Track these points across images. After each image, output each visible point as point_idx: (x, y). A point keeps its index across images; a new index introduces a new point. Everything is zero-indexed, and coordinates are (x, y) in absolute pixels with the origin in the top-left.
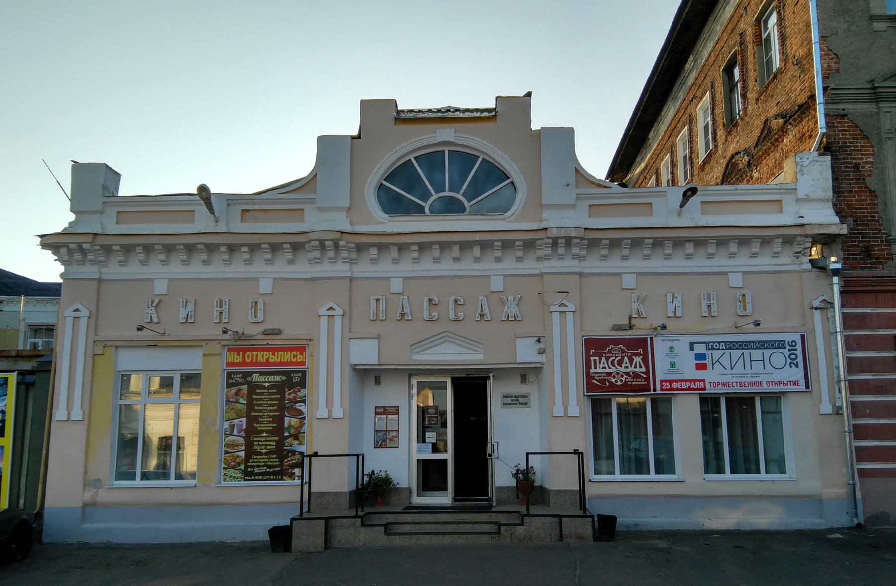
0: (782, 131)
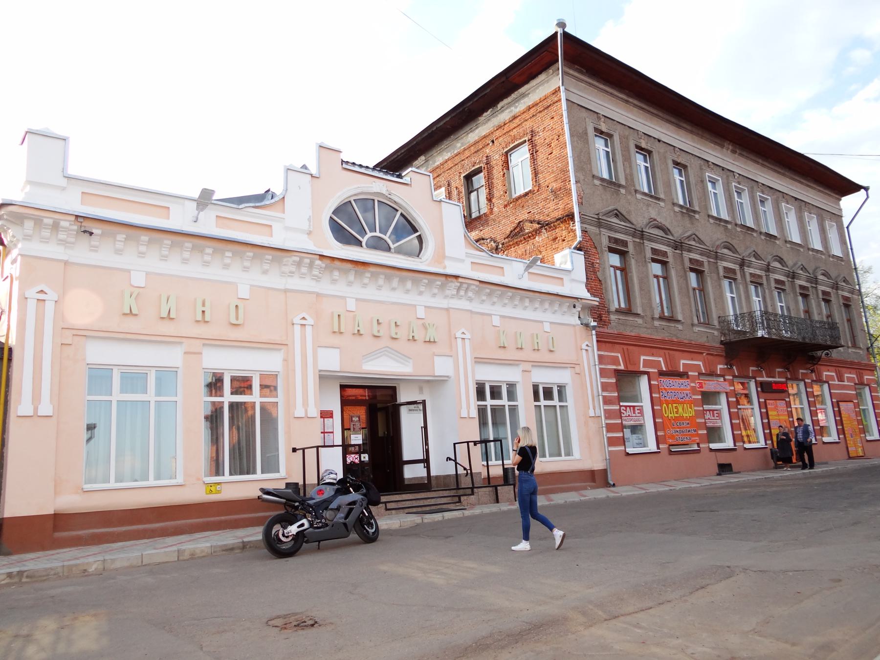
0: (536, 233)
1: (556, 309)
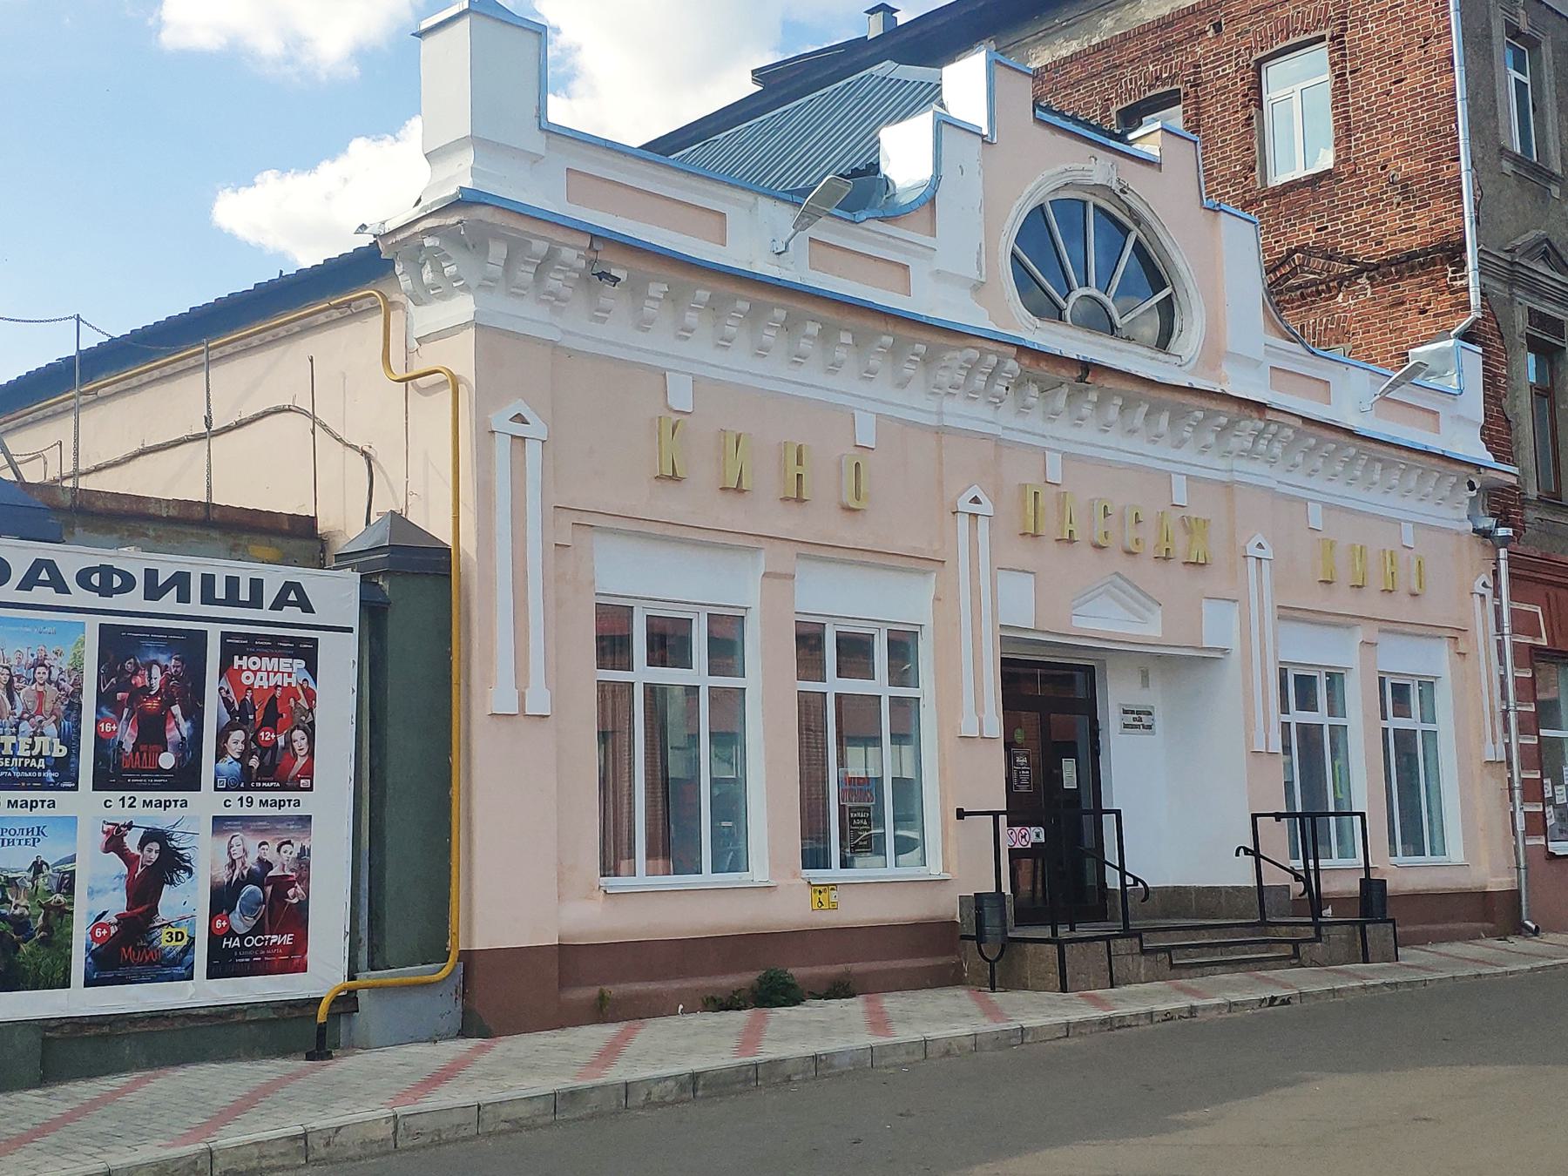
1: (1395, 482)
